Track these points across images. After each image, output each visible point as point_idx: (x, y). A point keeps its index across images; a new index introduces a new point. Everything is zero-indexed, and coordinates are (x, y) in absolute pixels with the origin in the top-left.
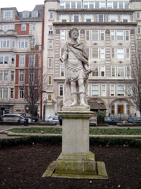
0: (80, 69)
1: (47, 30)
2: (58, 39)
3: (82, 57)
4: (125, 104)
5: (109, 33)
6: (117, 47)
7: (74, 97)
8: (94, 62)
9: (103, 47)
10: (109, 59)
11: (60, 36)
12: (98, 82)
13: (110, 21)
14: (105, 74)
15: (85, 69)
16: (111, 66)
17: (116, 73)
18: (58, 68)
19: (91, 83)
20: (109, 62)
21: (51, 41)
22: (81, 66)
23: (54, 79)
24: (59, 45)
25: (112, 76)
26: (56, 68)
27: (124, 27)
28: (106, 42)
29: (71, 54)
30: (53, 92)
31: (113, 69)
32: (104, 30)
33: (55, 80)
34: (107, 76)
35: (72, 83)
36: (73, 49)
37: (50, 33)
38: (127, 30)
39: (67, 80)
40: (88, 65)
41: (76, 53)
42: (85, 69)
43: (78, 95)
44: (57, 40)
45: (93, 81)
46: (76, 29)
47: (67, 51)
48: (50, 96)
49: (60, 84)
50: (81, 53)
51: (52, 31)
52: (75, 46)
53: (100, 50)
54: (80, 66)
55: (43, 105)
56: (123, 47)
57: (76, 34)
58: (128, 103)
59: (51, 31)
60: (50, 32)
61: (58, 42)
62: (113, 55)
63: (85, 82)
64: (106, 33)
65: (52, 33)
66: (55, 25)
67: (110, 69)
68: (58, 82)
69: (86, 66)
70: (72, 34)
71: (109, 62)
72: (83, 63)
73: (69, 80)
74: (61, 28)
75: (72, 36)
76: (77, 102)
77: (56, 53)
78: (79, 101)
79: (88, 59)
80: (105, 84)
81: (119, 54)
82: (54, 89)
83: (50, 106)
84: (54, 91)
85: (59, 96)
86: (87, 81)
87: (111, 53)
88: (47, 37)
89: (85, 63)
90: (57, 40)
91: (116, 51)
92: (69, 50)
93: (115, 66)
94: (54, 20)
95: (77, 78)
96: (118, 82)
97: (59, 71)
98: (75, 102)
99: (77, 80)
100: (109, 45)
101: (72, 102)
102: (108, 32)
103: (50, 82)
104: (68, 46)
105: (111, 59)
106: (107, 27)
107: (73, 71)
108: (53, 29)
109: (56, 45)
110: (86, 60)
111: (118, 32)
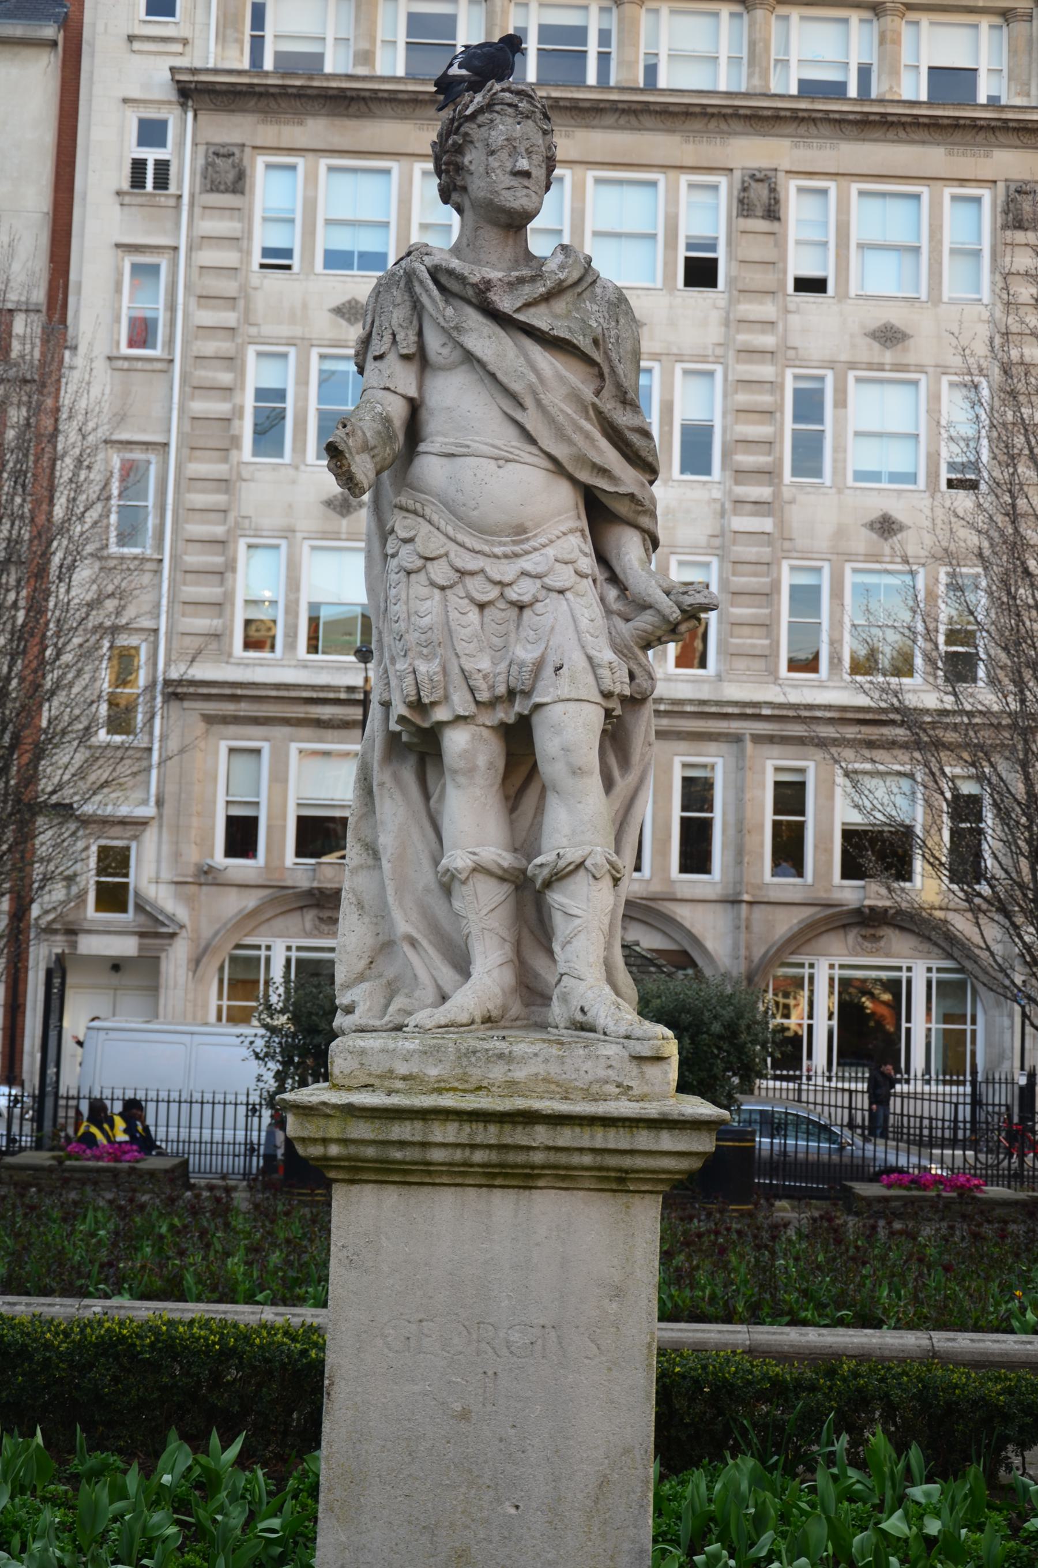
0: (564, 576)
1: (108, 144)
2: (228, 257)
3: (587, 436)
4: (920, 971)
5: (773, 212)
6: (853, 366)
7: (485, 915)
8: (871, 526)
9: (703, 359)
10: (762, 492)
11: (243, 214)
12: (244, 709)
13: (785, 83)
14: (719, 652)
15: (614, 579)
16: (785, 565)
17: (835, 643)
18: (216, 560)
19: (286, 722)
20: (766, 524)
21: (146, 272)
22: (577, 546)
23: (167, 683)
24: (230, 318)
25: (794, 665)
26: (194, 559)
27: (933, 157)
28: (732, 302)
29: (453, 397)
30: (143, 823)
31: (805, 598)
32: (722, 181)
33: (177, 692)
34: (741, 664)
35: (457, 742)
36: (485, 340)
37: (137, 179)
38: (963, 181)
39: (399, 709)
40: (653, 542)
41: (516, 387)
42: (614, 579)
43: (532, 899)
44: (209, 257)
45: (831, 721)
46: (523, 105)
47: (406, 358)
48: (114, 861)
49: (232, 729)
50: (575, 397)
51: (162, 167)
52: (506, 303)
53: (668, 386)
54: (566, 543)
55: (39, 957)
56: (921, 369)
57: (523, 164)
58: (950, 956)
59: (151, 155)
60: (138, 166)
61: (228, 287)
62: (808, 454)
63: (615, 738)
64: (744, 207)
65: (162, 181)
66: (195, 92)
67: (768, 595)
68: (213, 708)
69: (629, 548)
70: (472, 158)
71: (766, 524)
72: (600, 512)
73: (419, 706)
74: (268, 133)
75: (477, 186)
76: (508, 977)
77: (200, 406)
78: (538, 962)
79: (650, 470)
80: (713, 747)
81: (874, 442)
82: (170, 788)
83: (116, 966)
84: (168, 810)
85: (219, 858)
86: (644, 725)
87: (789, 425)
88: (103, 219)
89: (622, 508)
90: (209, 257)
91: (841, 402)
92: (434, 342)
93: (826, 568)
94: (185, 42)
95: (527, 694)
96: (850, 732)
97: (776, 616)
98: (489, 978)
99: (520, 707)
100: (768, 341)
101: (447, 974)
102: (760, 202)
103: (120, 719)
104: (431, 297)
105: (787, 493)
106: (752, 151)
107: (482, 606)
108: (181, 144)
109: (207, 317)
110: (629, 478)
111: (874, 205)
